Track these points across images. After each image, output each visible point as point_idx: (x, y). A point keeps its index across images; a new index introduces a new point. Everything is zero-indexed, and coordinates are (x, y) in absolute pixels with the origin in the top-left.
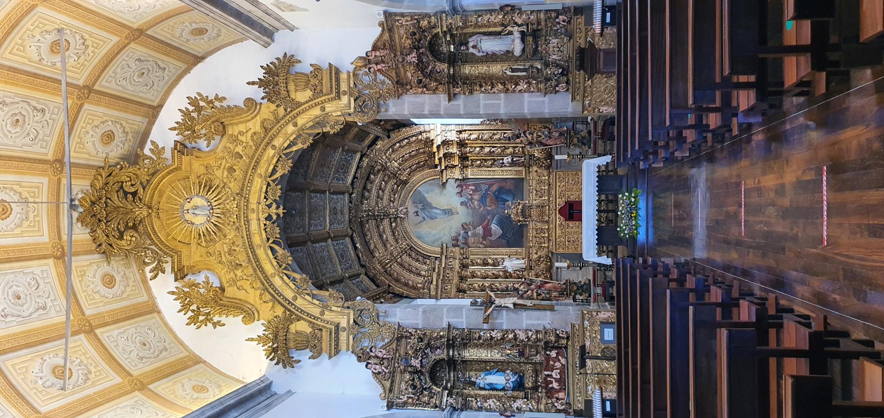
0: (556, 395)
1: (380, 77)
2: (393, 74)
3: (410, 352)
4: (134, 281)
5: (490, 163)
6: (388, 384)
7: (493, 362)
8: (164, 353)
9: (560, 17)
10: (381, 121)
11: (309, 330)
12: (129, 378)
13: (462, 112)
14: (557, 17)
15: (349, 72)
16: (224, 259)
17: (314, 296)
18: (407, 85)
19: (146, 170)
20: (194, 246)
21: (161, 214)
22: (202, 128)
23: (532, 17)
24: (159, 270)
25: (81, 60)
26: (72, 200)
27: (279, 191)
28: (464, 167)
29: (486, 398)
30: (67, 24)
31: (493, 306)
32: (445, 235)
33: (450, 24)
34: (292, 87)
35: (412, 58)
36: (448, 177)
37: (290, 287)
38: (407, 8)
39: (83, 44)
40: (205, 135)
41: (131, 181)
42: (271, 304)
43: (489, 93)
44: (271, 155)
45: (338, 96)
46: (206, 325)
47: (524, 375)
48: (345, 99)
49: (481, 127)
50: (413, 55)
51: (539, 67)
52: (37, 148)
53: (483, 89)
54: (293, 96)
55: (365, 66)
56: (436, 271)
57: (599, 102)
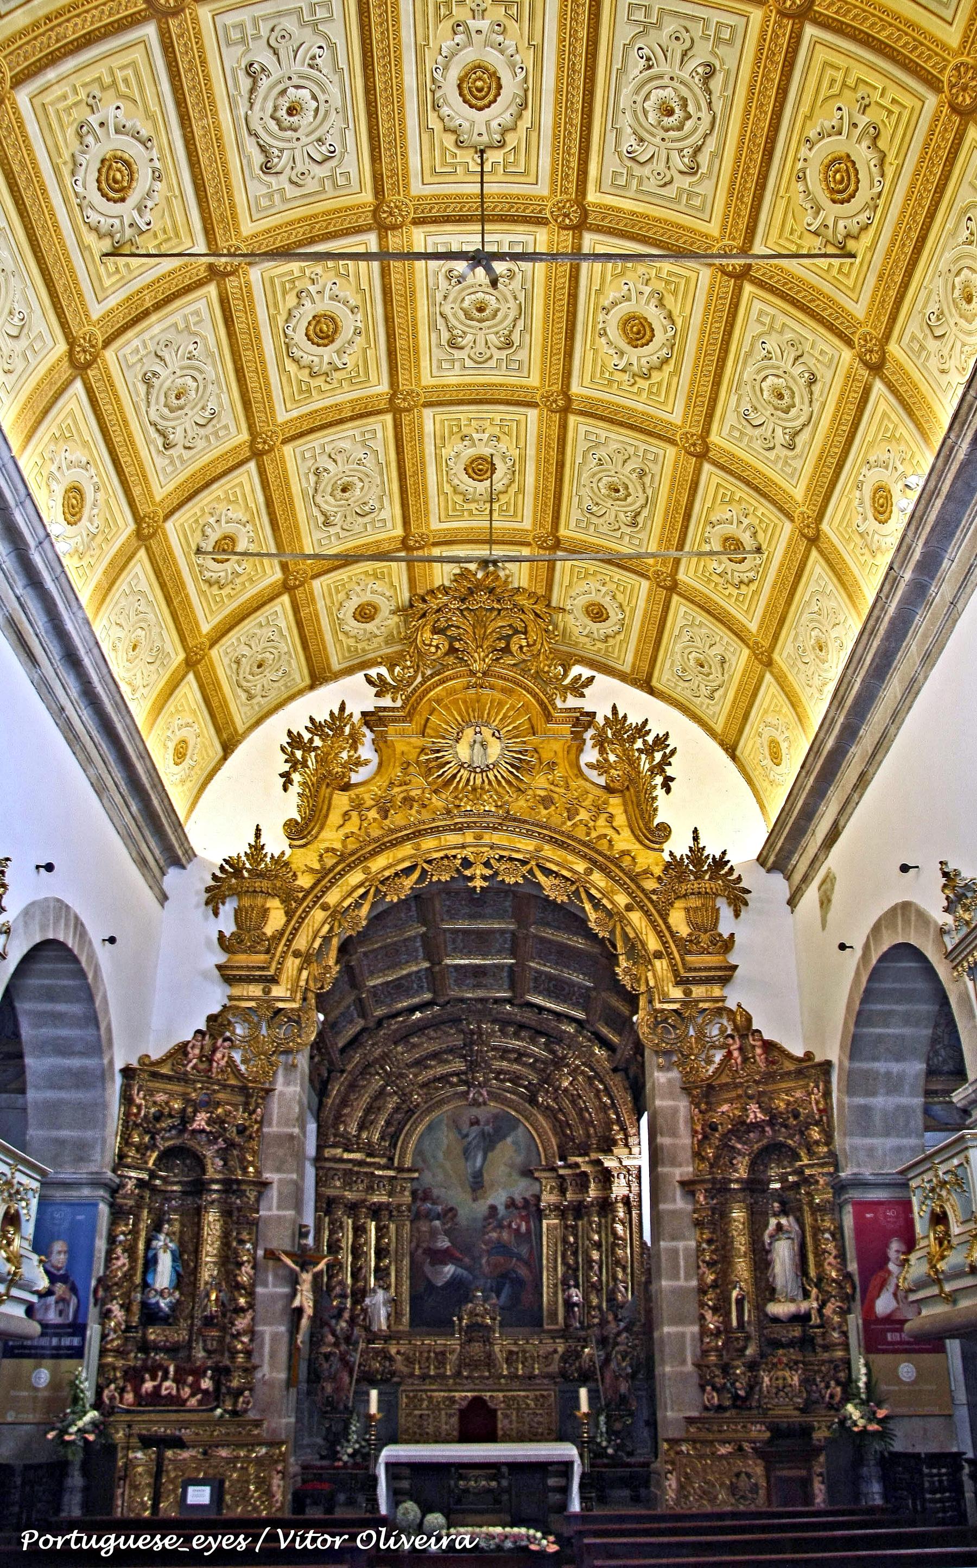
0: (129, 1388)
1: (718, 1056)
2: (725, 1079)
3: (220, 1110)
4: (364, 650)
5: (571, 1262)
6: (165, 1070)
7: (196, 1268)
8: (243, 696)
9: (839, 1389)
10: (643, 1055)
11: (269, 930)
12: (208, 644)
13: (662, 1206)
14: (838, 1383)
15: (723, 1001)
16: (397, 790)
17: (327, 939)
18: (707, 1103)
19: (546, 669)
20: (418, 742)
21: (472, 691)
22: (617, 756)
23: (836, 1335)
24: (381, 687)
25: (715, 578)
26: (495, 563)
27: (512, 881)
28: (563, 1211)
29: (131, 1251)
30: (769, 560)
31: (297, 1269)
32: (434, 1176)
33: (817, 1182)
34: (694, 902)
35: (755, 1113)
36: (544, 1182)
37: (345, 899)
38: (838, 1100)
39: (741, 582)
40: (606, 760)
41: (528, 645)
42: (317, 866)
43: (698, 1257)
44: (575, 867)
45: (680, 981)
46: (286, 761)
47: (170, 1325)
48: (677, 993)
49: (636, 1243)
50: (759, 1115)
51: (749, 1352)
52: (576, 514)
53: (704, 1246)
54: (679, 904)
55: (736, 1028)
56: (368, 1160)
57: (686, 1473)
